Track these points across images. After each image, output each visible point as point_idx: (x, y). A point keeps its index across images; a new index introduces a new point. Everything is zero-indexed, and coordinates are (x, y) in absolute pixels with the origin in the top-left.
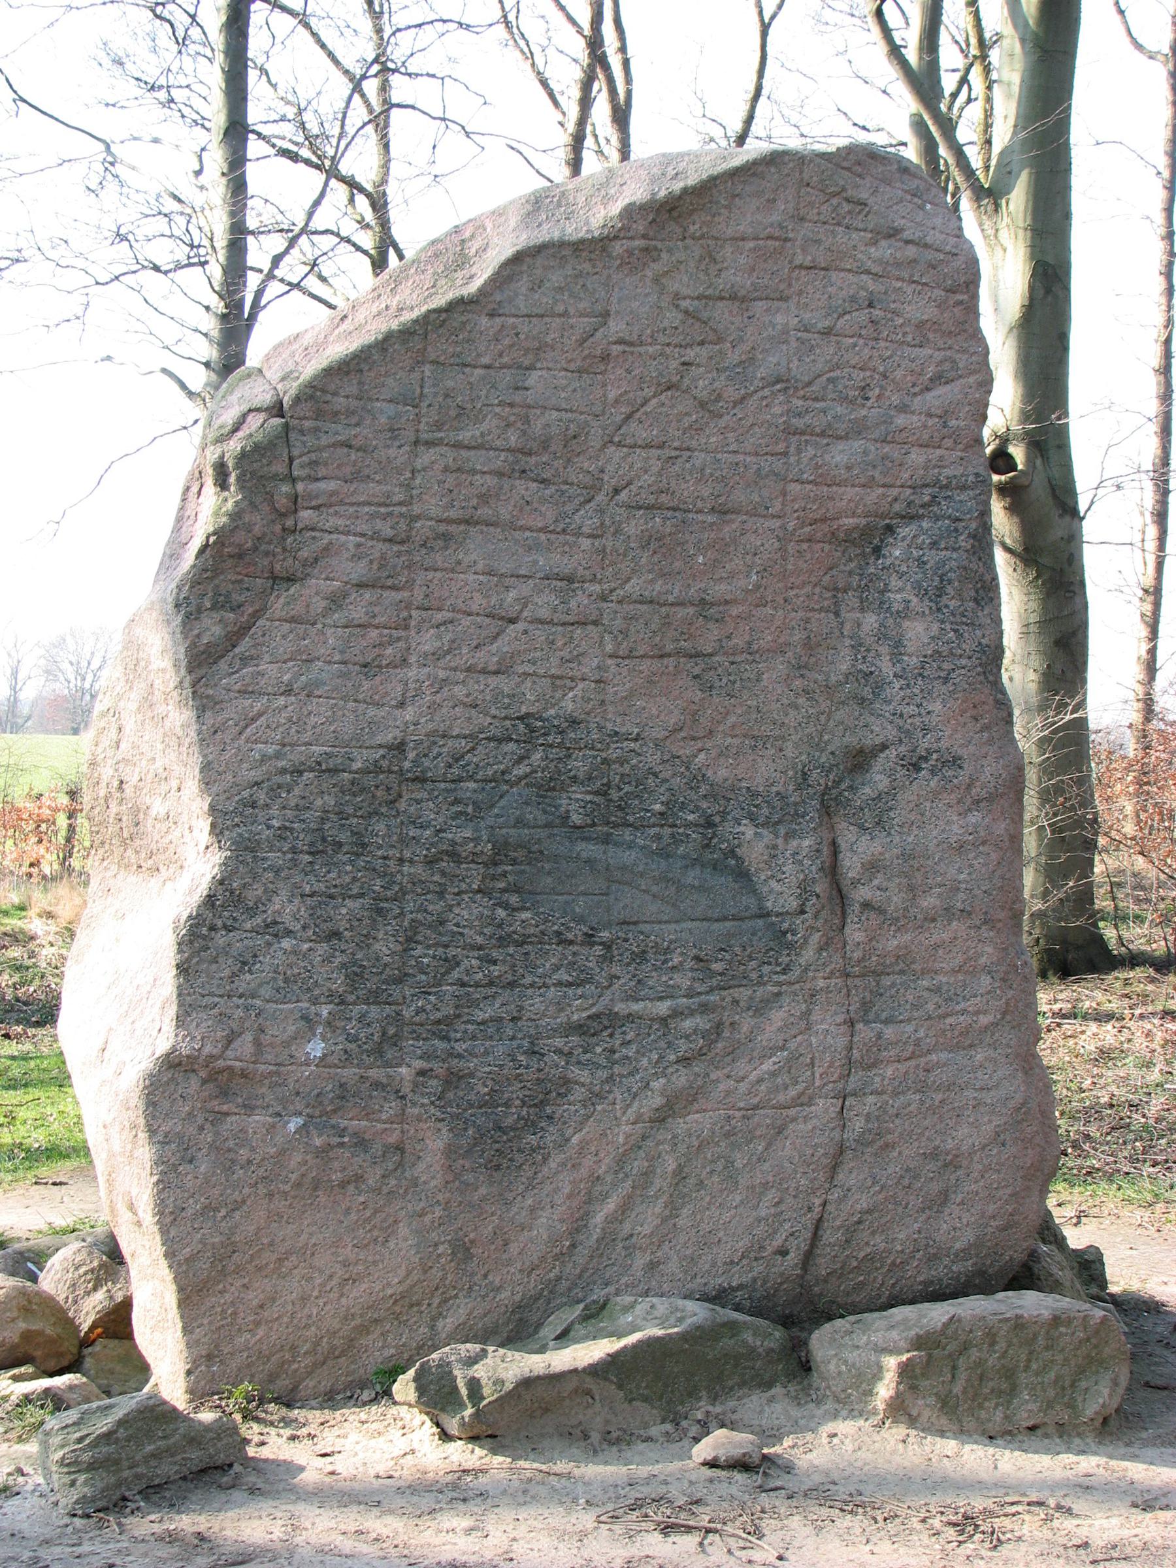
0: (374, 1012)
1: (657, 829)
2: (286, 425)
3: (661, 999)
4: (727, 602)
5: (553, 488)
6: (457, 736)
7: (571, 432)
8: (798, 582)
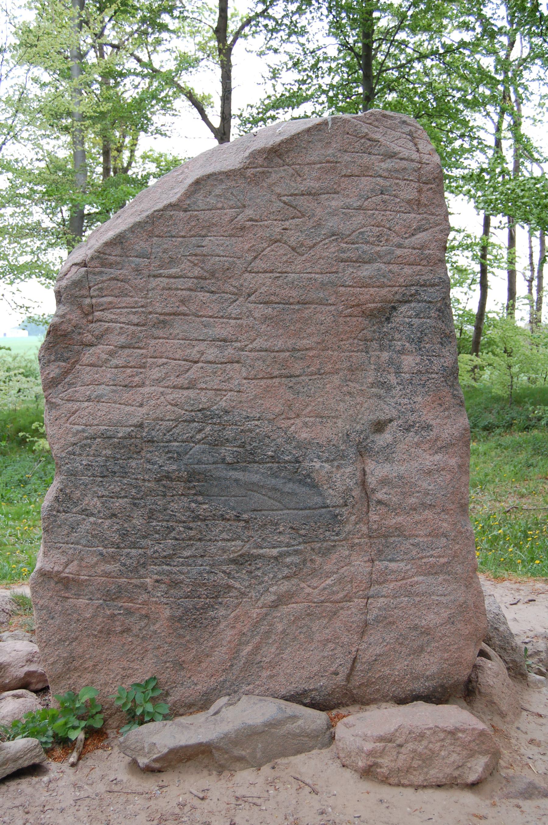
0: (134, 552)
1: (270, 465)
2: (87, 272)
3: (274, 548)
4: (307, 349)
5: (217, 295)
6: (168, 420)
7: (225, 267)
8: (345, 337)
